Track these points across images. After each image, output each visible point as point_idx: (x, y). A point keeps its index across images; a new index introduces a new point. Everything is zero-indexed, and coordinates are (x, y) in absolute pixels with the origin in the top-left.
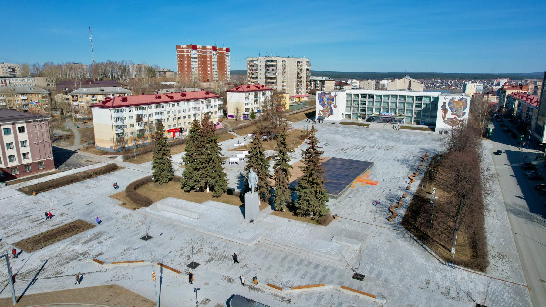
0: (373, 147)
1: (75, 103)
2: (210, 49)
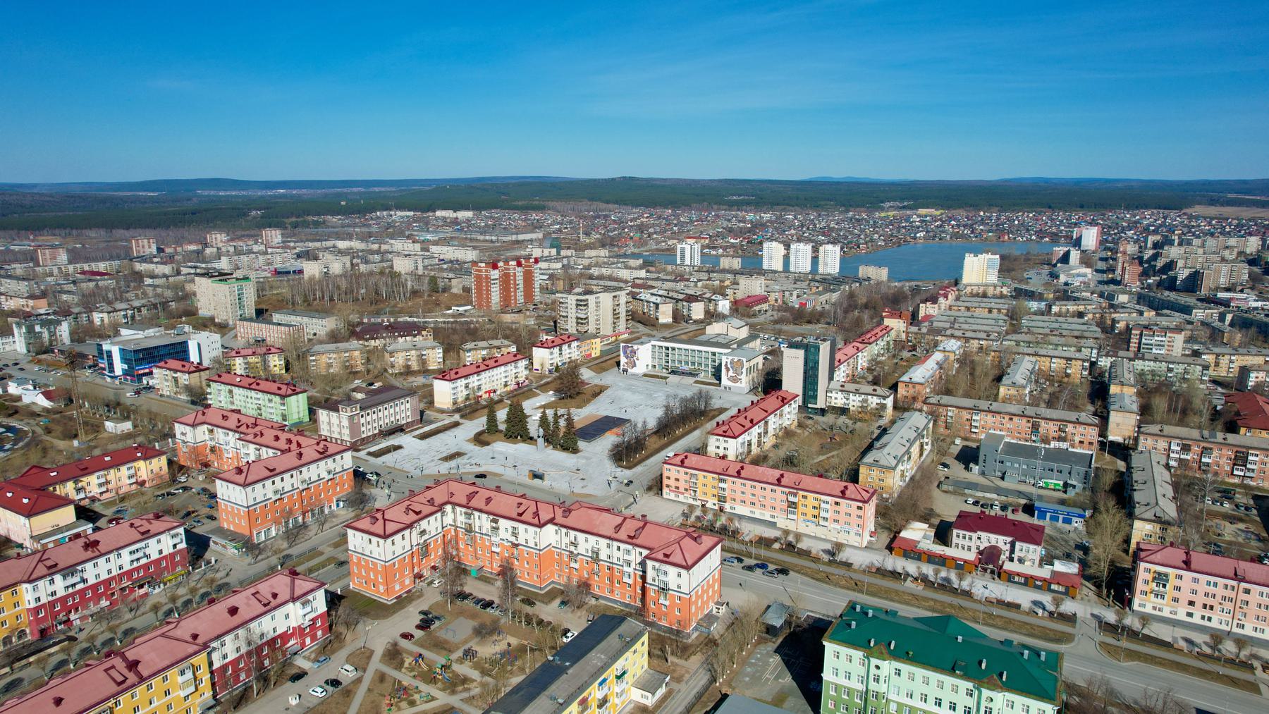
1: (392, 359)
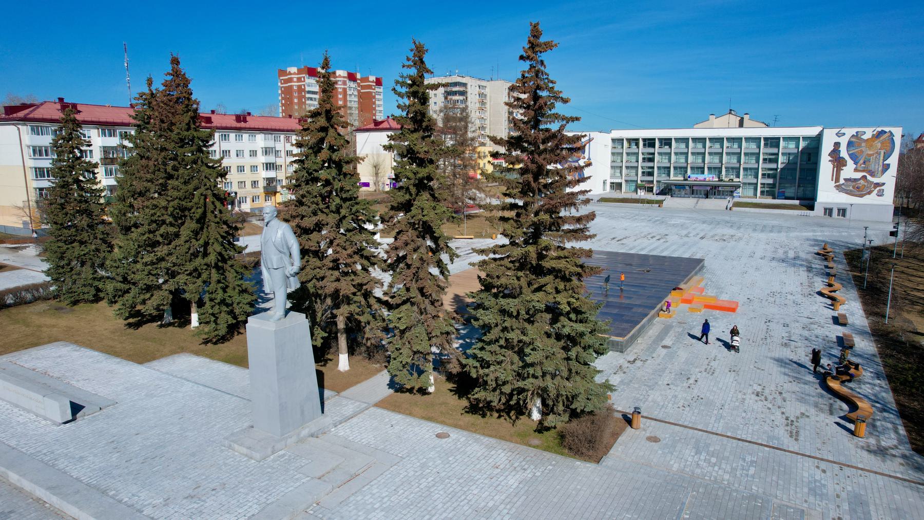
0: (687, 236)
2: (344, 77)
